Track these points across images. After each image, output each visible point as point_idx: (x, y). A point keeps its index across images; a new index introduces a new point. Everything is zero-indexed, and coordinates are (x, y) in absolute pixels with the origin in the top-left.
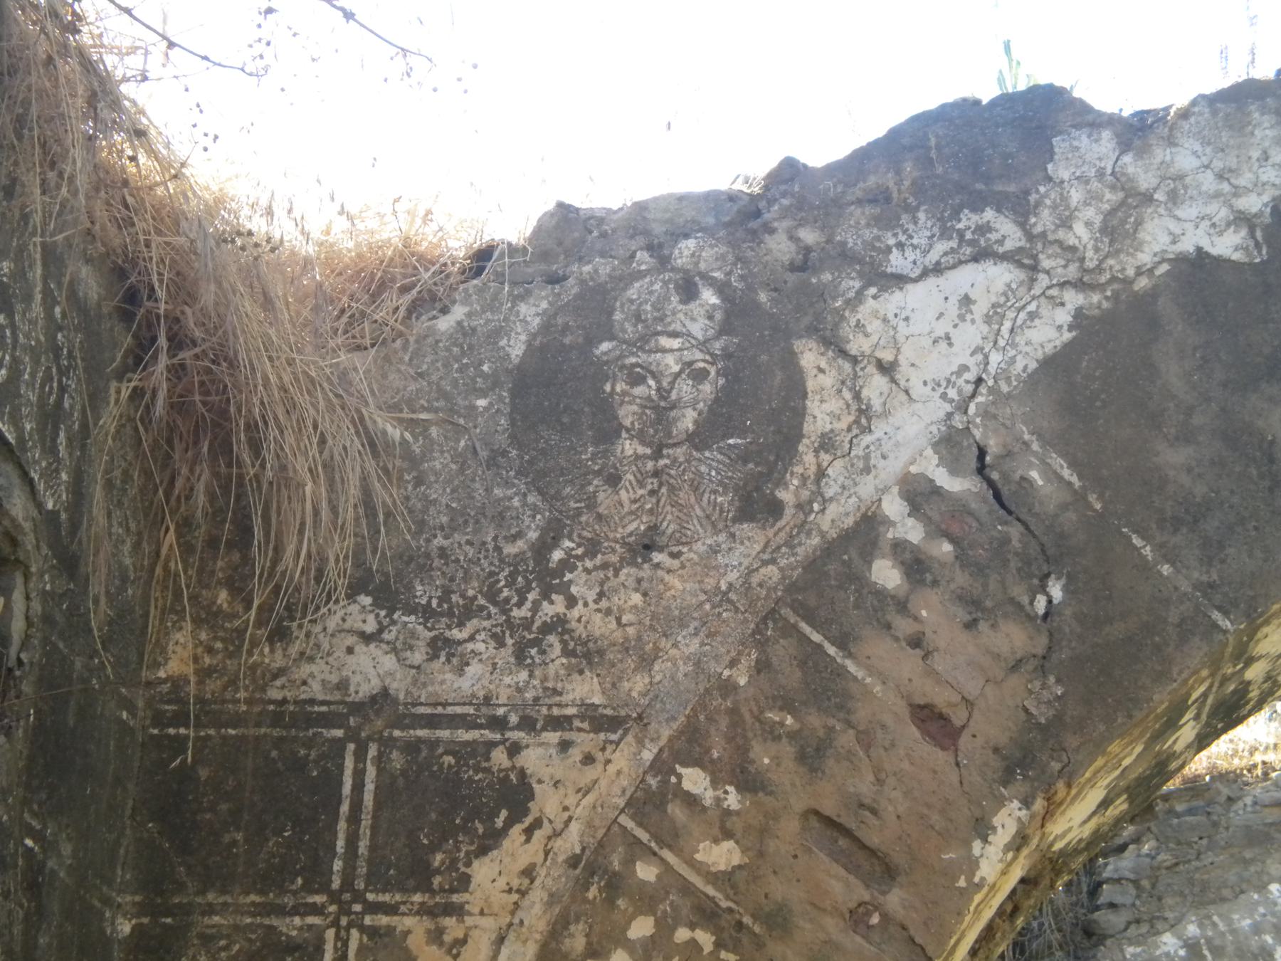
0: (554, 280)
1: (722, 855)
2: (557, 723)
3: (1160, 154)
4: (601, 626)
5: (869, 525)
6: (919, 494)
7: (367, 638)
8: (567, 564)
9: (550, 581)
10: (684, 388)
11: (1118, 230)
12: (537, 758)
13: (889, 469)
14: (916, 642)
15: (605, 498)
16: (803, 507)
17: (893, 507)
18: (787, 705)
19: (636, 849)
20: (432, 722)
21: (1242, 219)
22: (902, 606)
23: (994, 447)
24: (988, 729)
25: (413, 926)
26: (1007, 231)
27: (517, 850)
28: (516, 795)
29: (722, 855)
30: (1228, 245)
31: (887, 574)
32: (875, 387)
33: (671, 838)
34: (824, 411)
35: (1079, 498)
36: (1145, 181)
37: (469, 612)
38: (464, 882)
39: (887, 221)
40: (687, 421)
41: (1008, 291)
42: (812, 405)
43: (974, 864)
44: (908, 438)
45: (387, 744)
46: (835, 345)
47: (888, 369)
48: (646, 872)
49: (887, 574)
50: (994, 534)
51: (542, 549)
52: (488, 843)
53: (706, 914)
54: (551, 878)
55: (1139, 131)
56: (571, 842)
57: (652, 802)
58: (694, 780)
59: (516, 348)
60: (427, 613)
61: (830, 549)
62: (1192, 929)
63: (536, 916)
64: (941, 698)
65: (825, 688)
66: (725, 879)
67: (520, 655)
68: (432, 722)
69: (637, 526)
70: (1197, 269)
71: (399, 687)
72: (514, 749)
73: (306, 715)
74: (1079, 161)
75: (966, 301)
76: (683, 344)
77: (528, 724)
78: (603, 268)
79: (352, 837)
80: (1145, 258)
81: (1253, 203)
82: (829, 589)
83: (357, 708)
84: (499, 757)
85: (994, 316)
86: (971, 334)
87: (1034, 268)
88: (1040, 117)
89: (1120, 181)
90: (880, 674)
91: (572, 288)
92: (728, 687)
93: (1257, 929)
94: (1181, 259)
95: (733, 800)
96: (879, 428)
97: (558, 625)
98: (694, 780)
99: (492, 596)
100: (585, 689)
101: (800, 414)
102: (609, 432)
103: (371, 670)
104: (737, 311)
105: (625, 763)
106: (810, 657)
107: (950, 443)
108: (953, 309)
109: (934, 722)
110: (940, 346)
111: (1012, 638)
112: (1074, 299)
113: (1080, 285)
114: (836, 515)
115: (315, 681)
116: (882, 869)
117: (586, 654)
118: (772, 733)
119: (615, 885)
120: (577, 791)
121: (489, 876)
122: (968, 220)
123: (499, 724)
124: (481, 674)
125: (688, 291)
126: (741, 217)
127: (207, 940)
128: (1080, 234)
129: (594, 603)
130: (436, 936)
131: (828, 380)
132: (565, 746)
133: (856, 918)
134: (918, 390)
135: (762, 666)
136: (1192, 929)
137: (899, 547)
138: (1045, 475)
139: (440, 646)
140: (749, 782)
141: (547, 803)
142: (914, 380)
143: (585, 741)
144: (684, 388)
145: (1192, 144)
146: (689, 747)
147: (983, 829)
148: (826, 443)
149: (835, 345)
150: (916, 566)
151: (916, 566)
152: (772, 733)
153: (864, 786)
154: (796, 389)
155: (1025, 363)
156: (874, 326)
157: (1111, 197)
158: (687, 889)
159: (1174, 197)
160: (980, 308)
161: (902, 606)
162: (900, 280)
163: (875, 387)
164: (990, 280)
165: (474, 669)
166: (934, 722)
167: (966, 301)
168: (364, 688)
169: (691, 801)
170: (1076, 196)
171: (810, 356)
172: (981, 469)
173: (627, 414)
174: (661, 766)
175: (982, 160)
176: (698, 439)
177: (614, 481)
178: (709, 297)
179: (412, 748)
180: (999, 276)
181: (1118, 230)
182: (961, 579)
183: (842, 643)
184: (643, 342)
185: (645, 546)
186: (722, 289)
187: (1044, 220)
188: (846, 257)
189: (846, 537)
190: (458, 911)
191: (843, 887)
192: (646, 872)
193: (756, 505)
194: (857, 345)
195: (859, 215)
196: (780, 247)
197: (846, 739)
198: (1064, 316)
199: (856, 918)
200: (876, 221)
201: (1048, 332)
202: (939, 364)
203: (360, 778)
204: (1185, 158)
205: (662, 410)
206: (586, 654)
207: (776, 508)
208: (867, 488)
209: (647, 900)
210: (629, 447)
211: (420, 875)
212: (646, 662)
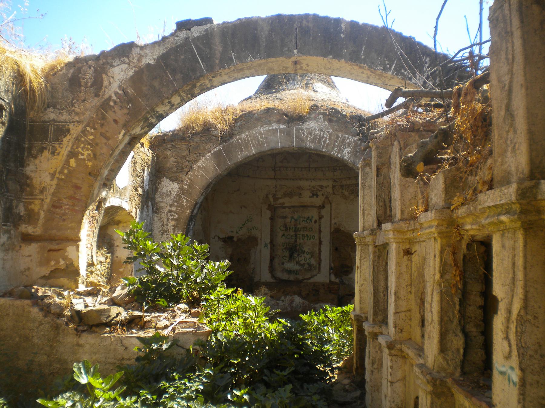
0: (75, 66)
1: (91, 137)
2: (73, 122)
3: (145, 50)
4: (78, 110)
5: (110, 98)
6: (116, 93)
7: (52, 112)
8: (75, 103)
9: (73, 105)
10: (89, 80)
11: (139, 60)
12: (71, 126)
13: (113, 90)
14: (114, 112)
15: (79, 94)
16: (103, 95)
17: (113, 95)
18: (99, 119)
19: (82, 137)
20: (59, 122)
21: (154, 59)
22: (113, 107)
23: (125, 87)
24: (121, 121)
25: (57, 146)
26: (127, 60)
27: (68, 137)
28: (68, 131)
29: (91, 137)
30: (152, 62)
31: (112, 103)
32: (112, 80)
33: (86, 135)
34: (105, 83)
35: (133, 94)
36: (143, 54)
37: (63, 109)
38: (62, 141)
39: (113, 59)
40: (89, 84)
41: (127, 68)
42: (104, 82)
43: (118, 137)
44: (115, 87)
45: (54, 125)
46: (107, 75)
47: (113, 78)
48: (83, 139)
49: (112, 103)
50: (125, 97)
51: (72, 101)
52: (65, 136)
53: (89, 144)
54: (72, 140)
55: (142, 48)
56: (74, 136)
57: (84, 132)
58: (88, 129)
59: (70, 76)
60: (59, 109)
61: (105, 100)
62: (247, 133)
63: (70, 144)
64: (117, 118)
65: (104, 118)
66: (91, 140)
67: (69, 114)
68: (59, 122)
69: (83, 98)
70: (148, 65)
71: (55, 118)
72: (68, 125)
73: (44, 122)
74: (135, 51)
75: (122, 69)
76: (89, 75)
77: (70, 123)
78: (80, 65)
79: (51, 136)
80: (142, 64)
81: (155, 57)
82: (105, 105)
83: (51, 121)
84: (67, 126)
85: (125, 71)
86: (122, 73)
87: (130, 65)
88: (132, 45)
89: (140, 54)
90: (110, 116)
91: (77, 67)
92: (93, 118)
93: (256, 133)
94: (146, 64)
95: (93, 131)
96: (112, 85)
97: (74, 110)
98: (88, 129)
99: (66, 107)
100: (77, 118)
101: (103, 83)
102: (80, 86)
103: (52, 116)
104: (96, 71)
105: (81, 127)
106: (102, 114)
107: (120, 87)
108: (120, 70)
109: (115, 121)
110: (119, 74)
111: (126, 111)
112: (134, 69)
113: (135, 67)
114: (106, 96)
115: (46, 118)
116: (108, 138)
117: (77, 114)
118: (98, 123)
119: (79, 141)
120: (75, 130)
121: (65, 140)
122: (122, 59)
123: (67, 122)
124: (65, 117)
125: (90, 68)
126: (97, 58)
127: (35, 147)
128: (135, 61)
129: (77, 108)
130: (59, 147)
131: (106, 79)
132: (74, 125)
133: (105, 144)
134: (116, 80)
135: (97, 115)
136: (247, 133)
137: (113, 100)
138: (130, 91)
139: (60, 113)
140: (95, 129)
141: (72, 132)
142: (116, 79)
143: (76, 124)
144: (89, 80)
145: (148, 49)
146: (88, 125)
147: (120, 133)
148: (106, 87)
149: (107, 75)
150: (115, 102)
151: (115, 102)
152: (98, 123)
153: (107, 129)
154: (102, 80)
155: (129, 77)
156: (111, 72)
157: (139, 56)
158: (87, 141)
159: (146, 56)
160: (124, 70)
161: (113, 107)
162: (114, 66)
163: (112, 80)
164: (124, 66)
165: (64, 116)
166: (115, 121)
167: (122, 69)
168: (52, 118)
169: (88, 131)
170: (135, 56)
171: (104, 76)
172: (123, 90)
173: (83, 84)
174: (85, 127)
175: (124, 51)
176: (91, 87)
177: (81, 92)
178: (92, 69)
179: (57, 125)
180: (126, 66)
181: (139, 60)
182: (120, 104)
183: (106, 112)
184: (85, 74)
185: (84, 101)
186: (94, 67)
187: (131, 59)
188: (108, 63)
189: (107, 99)
190: (62, 144)
191: (104, 140)
192: (83, 139)
193: (97, 95)
194: (109, 75)
195: (110, 58)
196: (101, 62)
197: (106, 124)
198: (133, 71)
199: (105, 144)
200: (112, 59)
201: (131, 73)
202: (119, 77)
203: (51, 129)
204: (147, 51)
205: (86, 83)
206: (77, 114)
207: (99, 95)
208: (110, 93)
209: (83, 142)
210: (82, 88)
211: (57, 140)
212: (84, 114)
